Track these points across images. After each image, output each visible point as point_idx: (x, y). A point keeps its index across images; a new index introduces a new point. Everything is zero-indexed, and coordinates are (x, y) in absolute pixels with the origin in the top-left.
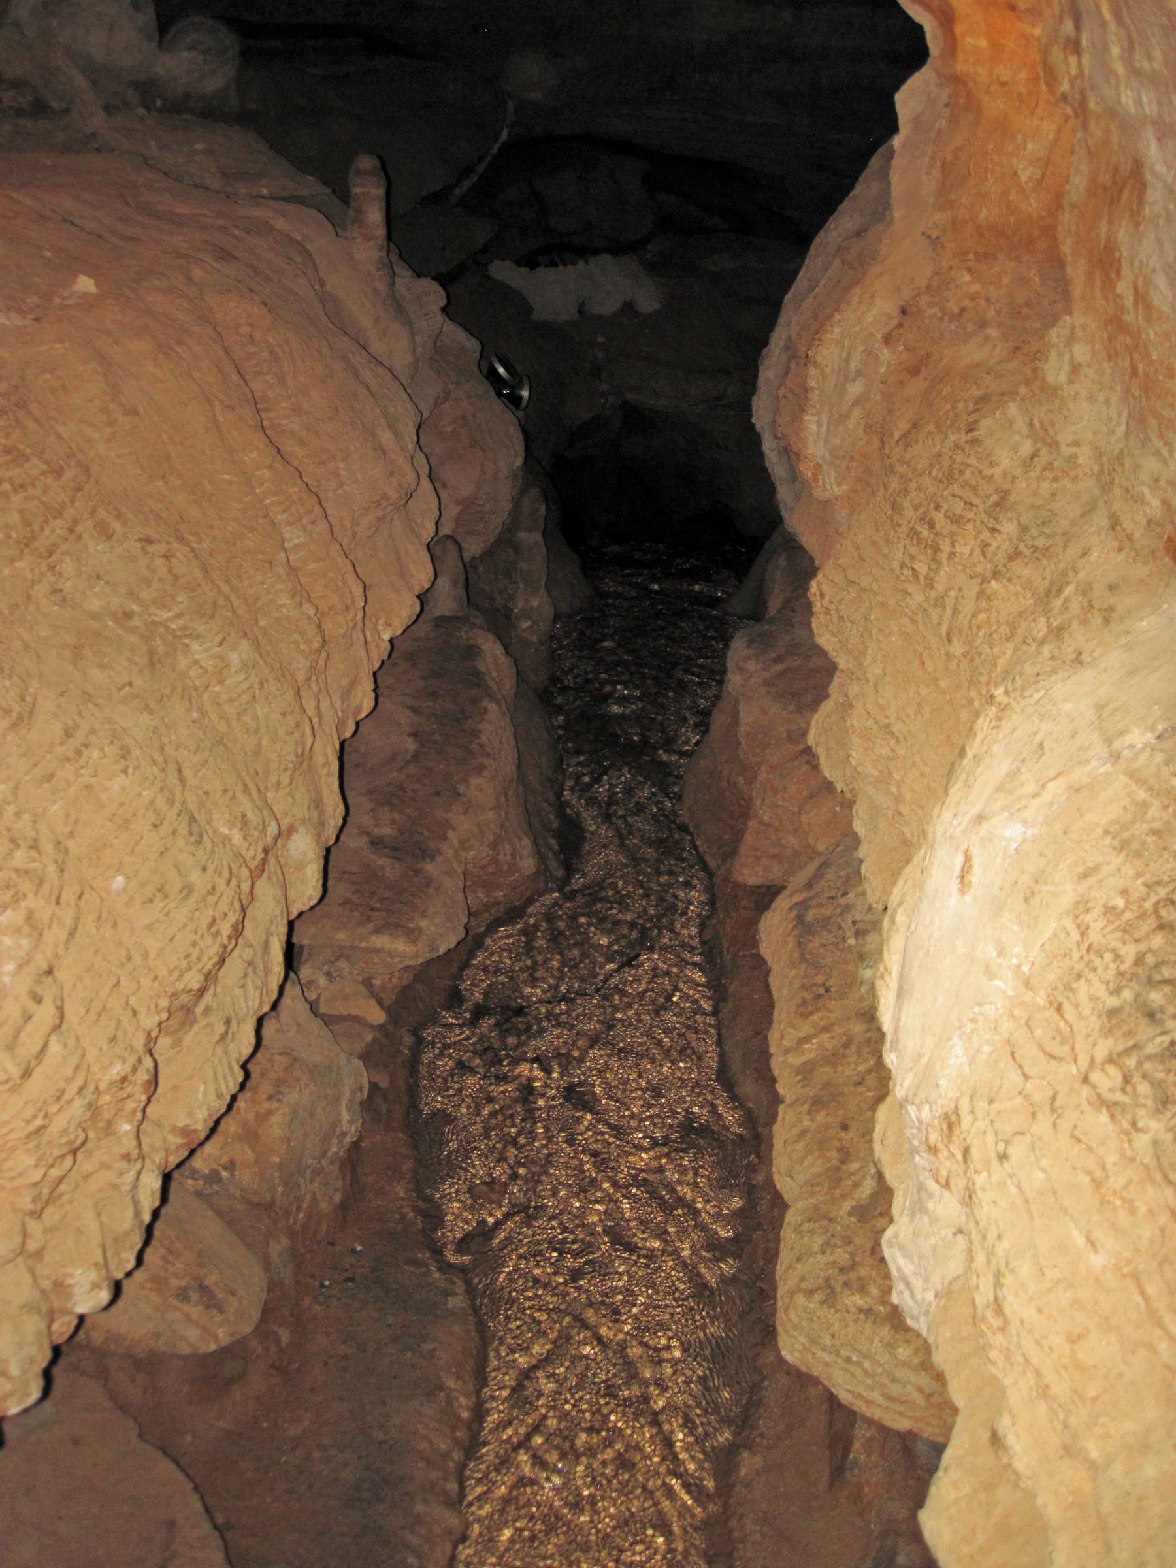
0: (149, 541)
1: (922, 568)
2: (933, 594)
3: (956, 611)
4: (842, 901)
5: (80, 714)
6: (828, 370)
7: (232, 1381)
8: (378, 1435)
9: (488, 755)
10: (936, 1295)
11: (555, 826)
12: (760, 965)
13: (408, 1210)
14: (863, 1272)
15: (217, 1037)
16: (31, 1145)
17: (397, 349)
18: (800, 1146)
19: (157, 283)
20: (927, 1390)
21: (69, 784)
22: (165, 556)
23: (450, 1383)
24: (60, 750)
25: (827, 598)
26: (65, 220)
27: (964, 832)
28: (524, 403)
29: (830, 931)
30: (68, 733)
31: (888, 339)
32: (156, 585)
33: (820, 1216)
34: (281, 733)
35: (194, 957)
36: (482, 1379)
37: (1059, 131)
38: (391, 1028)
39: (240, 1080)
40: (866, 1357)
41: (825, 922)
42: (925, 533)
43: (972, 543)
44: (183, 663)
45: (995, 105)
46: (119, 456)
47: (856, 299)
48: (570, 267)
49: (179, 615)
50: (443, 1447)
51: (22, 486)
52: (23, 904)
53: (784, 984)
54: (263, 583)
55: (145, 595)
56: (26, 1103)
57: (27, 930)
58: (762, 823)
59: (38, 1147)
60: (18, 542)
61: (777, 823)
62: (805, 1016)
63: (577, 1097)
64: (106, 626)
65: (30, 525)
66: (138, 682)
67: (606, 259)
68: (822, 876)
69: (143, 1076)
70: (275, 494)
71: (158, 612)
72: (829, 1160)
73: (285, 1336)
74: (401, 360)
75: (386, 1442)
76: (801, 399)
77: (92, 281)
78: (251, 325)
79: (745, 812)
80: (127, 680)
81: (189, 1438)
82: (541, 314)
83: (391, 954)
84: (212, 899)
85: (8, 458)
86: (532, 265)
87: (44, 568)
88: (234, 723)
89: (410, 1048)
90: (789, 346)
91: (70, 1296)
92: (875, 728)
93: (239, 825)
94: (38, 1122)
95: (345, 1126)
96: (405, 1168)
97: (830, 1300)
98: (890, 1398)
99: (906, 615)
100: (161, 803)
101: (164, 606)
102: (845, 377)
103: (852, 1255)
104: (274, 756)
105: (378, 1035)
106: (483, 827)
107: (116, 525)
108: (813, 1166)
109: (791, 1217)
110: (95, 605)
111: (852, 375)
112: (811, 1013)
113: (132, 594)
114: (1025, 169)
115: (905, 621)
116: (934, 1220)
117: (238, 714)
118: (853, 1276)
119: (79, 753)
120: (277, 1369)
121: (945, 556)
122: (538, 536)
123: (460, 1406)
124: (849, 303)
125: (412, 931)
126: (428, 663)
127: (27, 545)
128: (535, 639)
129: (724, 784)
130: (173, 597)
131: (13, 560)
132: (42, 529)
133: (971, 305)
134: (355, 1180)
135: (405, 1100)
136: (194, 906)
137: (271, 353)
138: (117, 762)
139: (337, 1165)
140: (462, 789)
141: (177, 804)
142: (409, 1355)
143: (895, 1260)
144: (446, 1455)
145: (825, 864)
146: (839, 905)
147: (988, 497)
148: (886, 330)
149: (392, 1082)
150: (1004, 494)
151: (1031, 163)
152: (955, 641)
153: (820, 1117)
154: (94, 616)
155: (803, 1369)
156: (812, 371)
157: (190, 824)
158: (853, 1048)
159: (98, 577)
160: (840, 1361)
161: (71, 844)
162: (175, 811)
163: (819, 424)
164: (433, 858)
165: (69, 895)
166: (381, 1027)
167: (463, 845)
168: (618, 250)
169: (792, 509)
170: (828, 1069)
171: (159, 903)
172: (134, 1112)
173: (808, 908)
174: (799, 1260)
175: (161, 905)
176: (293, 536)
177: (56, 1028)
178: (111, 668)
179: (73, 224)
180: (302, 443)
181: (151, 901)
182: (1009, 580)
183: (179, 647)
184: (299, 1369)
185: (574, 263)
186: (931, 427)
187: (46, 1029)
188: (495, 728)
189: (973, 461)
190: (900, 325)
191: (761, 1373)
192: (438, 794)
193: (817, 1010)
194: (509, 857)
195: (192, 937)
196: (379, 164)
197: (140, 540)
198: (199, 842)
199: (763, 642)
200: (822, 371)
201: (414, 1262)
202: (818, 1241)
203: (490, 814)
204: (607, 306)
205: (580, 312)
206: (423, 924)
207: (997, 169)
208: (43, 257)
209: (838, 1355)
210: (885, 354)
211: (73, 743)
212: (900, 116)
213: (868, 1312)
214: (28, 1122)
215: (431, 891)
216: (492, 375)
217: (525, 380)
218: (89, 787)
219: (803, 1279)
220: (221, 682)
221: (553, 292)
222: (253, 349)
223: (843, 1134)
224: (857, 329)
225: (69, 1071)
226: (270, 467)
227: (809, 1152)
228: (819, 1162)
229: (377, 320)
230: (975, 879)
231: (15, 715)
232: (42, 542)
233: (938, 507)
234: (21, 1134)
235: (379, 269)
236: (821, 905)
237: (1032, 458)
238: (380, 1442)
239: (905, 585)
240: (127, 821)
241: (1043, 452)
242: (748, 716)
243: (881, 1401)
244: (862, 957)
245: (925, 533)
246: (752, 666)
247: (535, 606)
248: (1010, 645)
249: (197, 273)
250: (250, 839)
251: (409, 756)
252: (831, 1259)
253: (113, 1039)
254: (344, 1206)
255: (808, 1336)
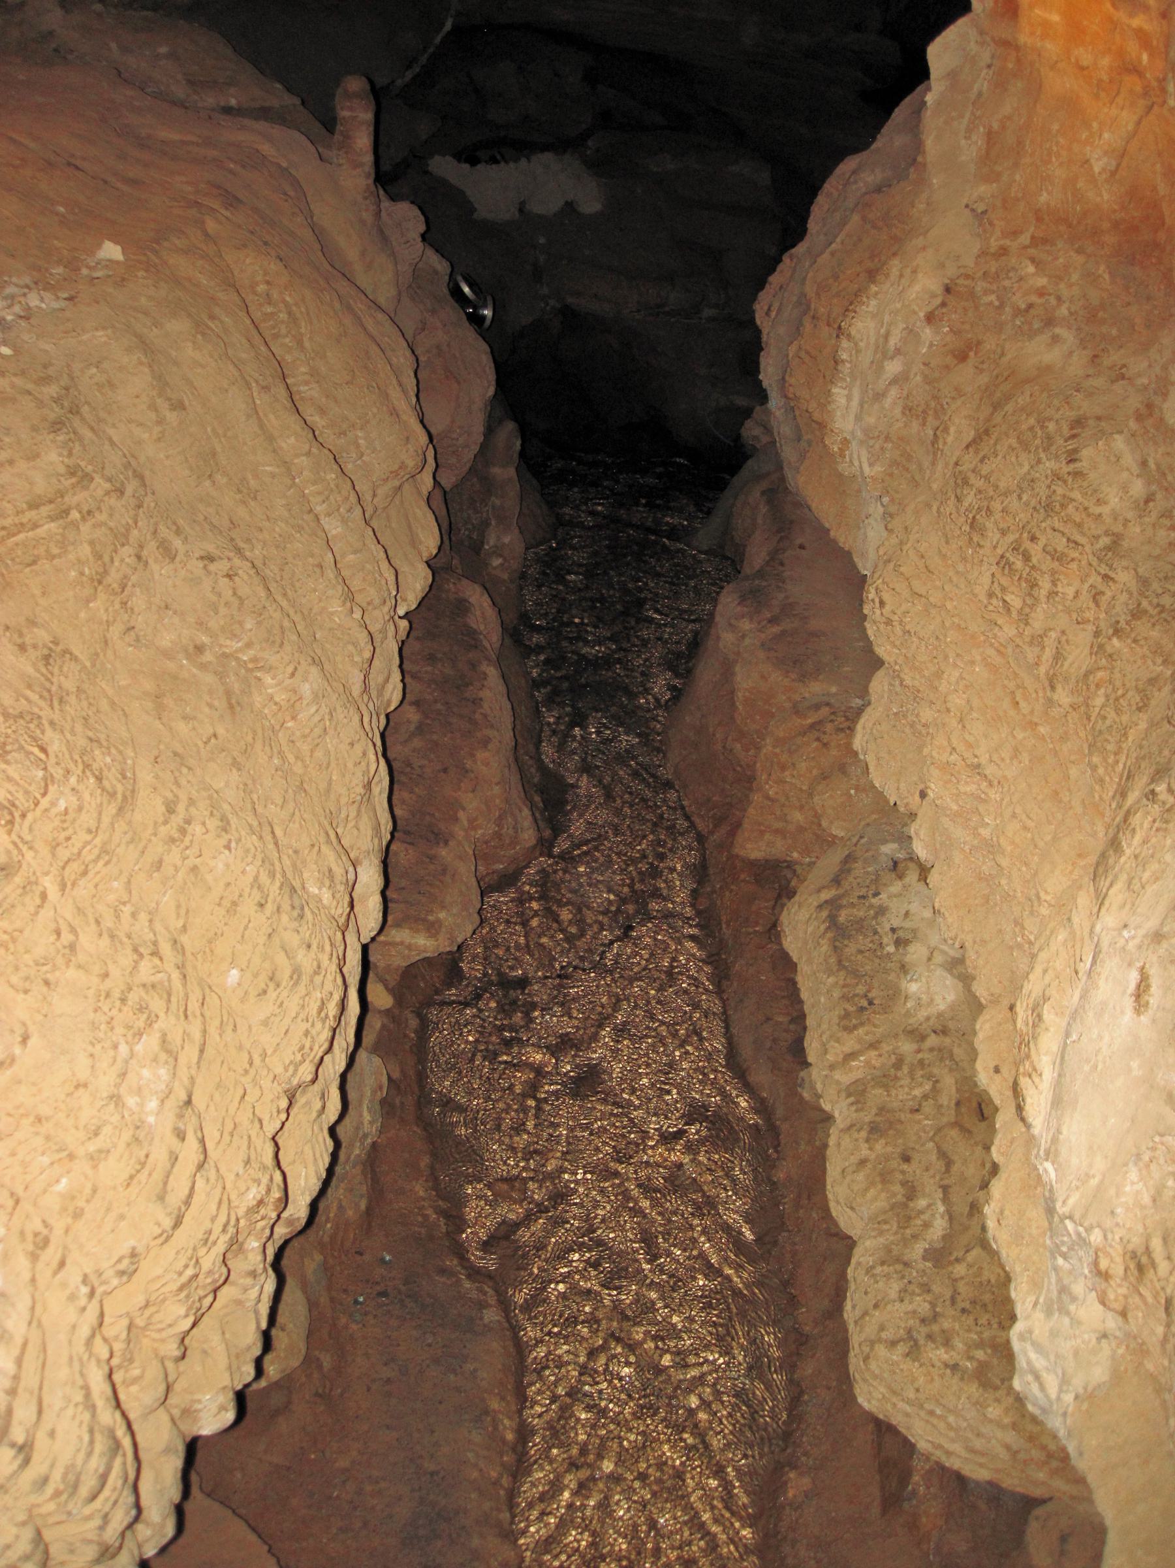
0: (211, 559)
1: (1015, 601)
2: (1028, 631)
3: (1058, 657)
4: (874, 901)
5: (177, 783)
6: (862, 344)
7: (276, 1413)
8: (430, 1466)
9: (492, 726)
10: (1077, 1397)
11: (536, 780)
12: (785, 964)
13: (429, 1212)
14: (946, 1324)
15: (314, 1114)
16: (183, 1295)
17: (381, 280)
18: (860, 1177)
19: (177, 242)
20: (1015, 1448)
21: (177, 870)
22: (229, 576)
23: (495, 1405)
24: (163, 830)
25: (888, 608)
26: (69, 164)
27: (1140, 947)
28: (488, 322)
29: (865, 936)
30: (170, 810)
31: (930, 318)
32: (223, 610)
33: (892, 1258)
34: (350, 765)
35: (307, 1050)
36: (522, 1399)
37: (1139, 123)
38: (396, 1011)
39: (331, 1150)
40: (950, 1411)
41: (860, 925)
42: (1019, 564)
43: (1077, 583)
44: (258, 699)
45: (1059, 83)
46: (167, 457)
47: (895, 272)
48: (512, 165)
49: (249, 645)
50: (494, 1474)
51: (89, 512)
52: (156, 1026)
53: (819, 989)
54: (315, 590)
55: (213, 624)
56: (178, 1253)
57: (163, 1056)
58: (768, 798)
59: (188, 1297)
60: (92, 580)
61: (783, 800)
62: (849, 1030)
63: (587, 1082)
64: (182, 666)
65: (100, 557)
66: (221, 731)
67: (548, 157)
68: (849, 871)
69: (277, 1194)
70: (315, 483)
71: (228, 642)
72: (894, 1195)
73: (327, 1361)
74: (386, 295)
75: (437, 1473)
76: (827, 369)
77: (119, 248)
78: (268, 283)
79: (747, 780)
80: (211, 731)
81: (239, 1475)
82: (483, 212)
83: (409, 947)
84: (318, 979)
85: (74, 480)
86: (473, 161)
87: (117, 606)
88: (308, 759)
89: (416, 1032)
90: (803, 304)
91: (195, 1420)
92: (960, 763)
93: (327, 883)
94: (190, 1272)
95: (366, 1127)
96: (422, 1165)
97: (914, 1352)
98: (972, 1451)
99: (992, 645)
100: (264, 878)
101: (234, 636)
102: (883, 354)
103: (933, 1305)
104: (344, 791)
105: (385, 1021)
106: (487, 802)
107: (177, 543)
108: (877, 1201)
109: (858, 1256)
110: (166, 640)
111: (890, 353)
112: (855, 1027)
113: (201, 624)
114: (1099, 159)
115: (991, 652)
116: (1076, 1322)
117: (312, 751)
118: (935, 1328)
119: (183, 831)
120: (320, 1396)
121: (1044, 592)
122: (511, 472)
123: (505, 1428)
124: (887, 276)
125: (432, 924)
126: (431, 631)
127: (100, 582)
128: (506, 576)
129: (719, 747)
130: (241, 623)
131: (88, 601)
132: (112, 561)
133: (1040, 301)
134: (375, 1180)
135: (416, 1090)
136: (304, 992)
137: (290, 313)
138: (219, 836)
139: (359, 1169)
140: (469, 764)
141: (278, 876)
142: (452, 1377)
143: (1026, 1354)
144: (496, 1483)
145: (849, 859)
146: (871, 906)
147: (1097, 538)
148: (929, 309)
149: (402, 1071)
150: (1117, 539)
151: (1106, 153)
152: (1059, 687)
153: (879, 1146)
154: (167, 654)
155: (881, 1416)
156: (845, 343)
157: (291, 898)
158: (905, 1069)
159: (167, 607)
160: (922, 1414)
161: (184, 939)
162: (278, 884)
163: (849, 398)
164: (446, 843)
165: (194, 1005)
166: (388, 1012)
167: (473, 825)
168: (561, 145)
169: (797, 470)
170: (878, 1091)
171: (272, 994)
172: (263, 1229)
173: (840, 907)
174: (876, 1306)
175: (274, 995)
176: (334, 527)
177: (200, 1166)
178: (194, 718)
179: (77, 168)
180: (322, 411)
181: (265, 992)
182: (1135, 641)
183: (253, 681)
184: (341, 1395)
185: (516, 160)
186: (1013, 441)
187: (192, 1168)
188: (492, 692)
189: (1076, 495)
190: (943, 304)
191: (799, 1385)
192: (445, 770)
193: (862, 1024)
194: (511, 831)
195: (305, 1026)
196: (368, 87)
197: (202, 558)
198: (301, 916)
199: (754, 598)
200: (856, 344)
201: (442, 1271)
202: (895, 1287)
203: (497, 790)
204: (547, 204)
205: (521, 211)
206: (442, 915)
207: (1064, 153)
208: (57, 214)
209: (921, 1407)
210: (927, 333)
211: (177, 819)
212: (932, 70)
213: (955, 1367)
214: (180, 1274)
215: (448, 879)
216: (457, 293)
217: (489, 298)
218: (194, 869)
219: (882, 1328)
220: (293, 718)
221: (494, 190)
222: (269, 310)
223: (905, 1167)
224: (899, 306)
225: (213, 1207)
226: (309, 454)
227: (872, 1184)
228: (883, 1195)
229: (363, 253)
230: (1155, 997)
231: (119, 796)
232: (113, 578)
233: (1033, 539)
234: (174, 1287)
235: (365, 198)
236: (853, 905)
237: (1147, 502)
238: (432, 1474)
239: (994, 616)
240: (235, 904)
241: (1159, 496)
242: (745, 681)
243: (964, 1453)
244: (904, 968)
245: (1019, 564)
246: (746, 625)
247: (506, 545)
248: (1144, 716)
249: (211, 225)
250: (338, 896)
251: (412, 727)
252: (910, 1308)
253: (248, 1162)
254: (369, 1211)
255: (889, 1387)
